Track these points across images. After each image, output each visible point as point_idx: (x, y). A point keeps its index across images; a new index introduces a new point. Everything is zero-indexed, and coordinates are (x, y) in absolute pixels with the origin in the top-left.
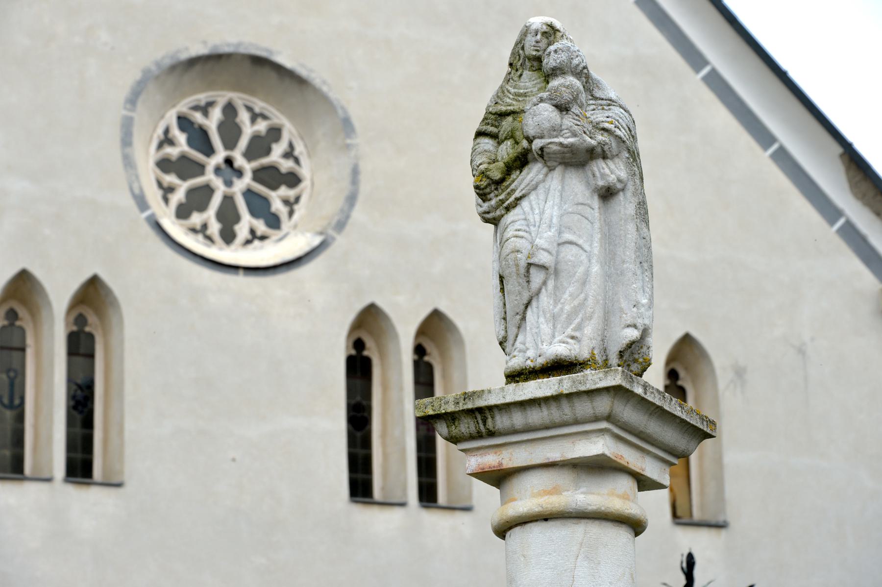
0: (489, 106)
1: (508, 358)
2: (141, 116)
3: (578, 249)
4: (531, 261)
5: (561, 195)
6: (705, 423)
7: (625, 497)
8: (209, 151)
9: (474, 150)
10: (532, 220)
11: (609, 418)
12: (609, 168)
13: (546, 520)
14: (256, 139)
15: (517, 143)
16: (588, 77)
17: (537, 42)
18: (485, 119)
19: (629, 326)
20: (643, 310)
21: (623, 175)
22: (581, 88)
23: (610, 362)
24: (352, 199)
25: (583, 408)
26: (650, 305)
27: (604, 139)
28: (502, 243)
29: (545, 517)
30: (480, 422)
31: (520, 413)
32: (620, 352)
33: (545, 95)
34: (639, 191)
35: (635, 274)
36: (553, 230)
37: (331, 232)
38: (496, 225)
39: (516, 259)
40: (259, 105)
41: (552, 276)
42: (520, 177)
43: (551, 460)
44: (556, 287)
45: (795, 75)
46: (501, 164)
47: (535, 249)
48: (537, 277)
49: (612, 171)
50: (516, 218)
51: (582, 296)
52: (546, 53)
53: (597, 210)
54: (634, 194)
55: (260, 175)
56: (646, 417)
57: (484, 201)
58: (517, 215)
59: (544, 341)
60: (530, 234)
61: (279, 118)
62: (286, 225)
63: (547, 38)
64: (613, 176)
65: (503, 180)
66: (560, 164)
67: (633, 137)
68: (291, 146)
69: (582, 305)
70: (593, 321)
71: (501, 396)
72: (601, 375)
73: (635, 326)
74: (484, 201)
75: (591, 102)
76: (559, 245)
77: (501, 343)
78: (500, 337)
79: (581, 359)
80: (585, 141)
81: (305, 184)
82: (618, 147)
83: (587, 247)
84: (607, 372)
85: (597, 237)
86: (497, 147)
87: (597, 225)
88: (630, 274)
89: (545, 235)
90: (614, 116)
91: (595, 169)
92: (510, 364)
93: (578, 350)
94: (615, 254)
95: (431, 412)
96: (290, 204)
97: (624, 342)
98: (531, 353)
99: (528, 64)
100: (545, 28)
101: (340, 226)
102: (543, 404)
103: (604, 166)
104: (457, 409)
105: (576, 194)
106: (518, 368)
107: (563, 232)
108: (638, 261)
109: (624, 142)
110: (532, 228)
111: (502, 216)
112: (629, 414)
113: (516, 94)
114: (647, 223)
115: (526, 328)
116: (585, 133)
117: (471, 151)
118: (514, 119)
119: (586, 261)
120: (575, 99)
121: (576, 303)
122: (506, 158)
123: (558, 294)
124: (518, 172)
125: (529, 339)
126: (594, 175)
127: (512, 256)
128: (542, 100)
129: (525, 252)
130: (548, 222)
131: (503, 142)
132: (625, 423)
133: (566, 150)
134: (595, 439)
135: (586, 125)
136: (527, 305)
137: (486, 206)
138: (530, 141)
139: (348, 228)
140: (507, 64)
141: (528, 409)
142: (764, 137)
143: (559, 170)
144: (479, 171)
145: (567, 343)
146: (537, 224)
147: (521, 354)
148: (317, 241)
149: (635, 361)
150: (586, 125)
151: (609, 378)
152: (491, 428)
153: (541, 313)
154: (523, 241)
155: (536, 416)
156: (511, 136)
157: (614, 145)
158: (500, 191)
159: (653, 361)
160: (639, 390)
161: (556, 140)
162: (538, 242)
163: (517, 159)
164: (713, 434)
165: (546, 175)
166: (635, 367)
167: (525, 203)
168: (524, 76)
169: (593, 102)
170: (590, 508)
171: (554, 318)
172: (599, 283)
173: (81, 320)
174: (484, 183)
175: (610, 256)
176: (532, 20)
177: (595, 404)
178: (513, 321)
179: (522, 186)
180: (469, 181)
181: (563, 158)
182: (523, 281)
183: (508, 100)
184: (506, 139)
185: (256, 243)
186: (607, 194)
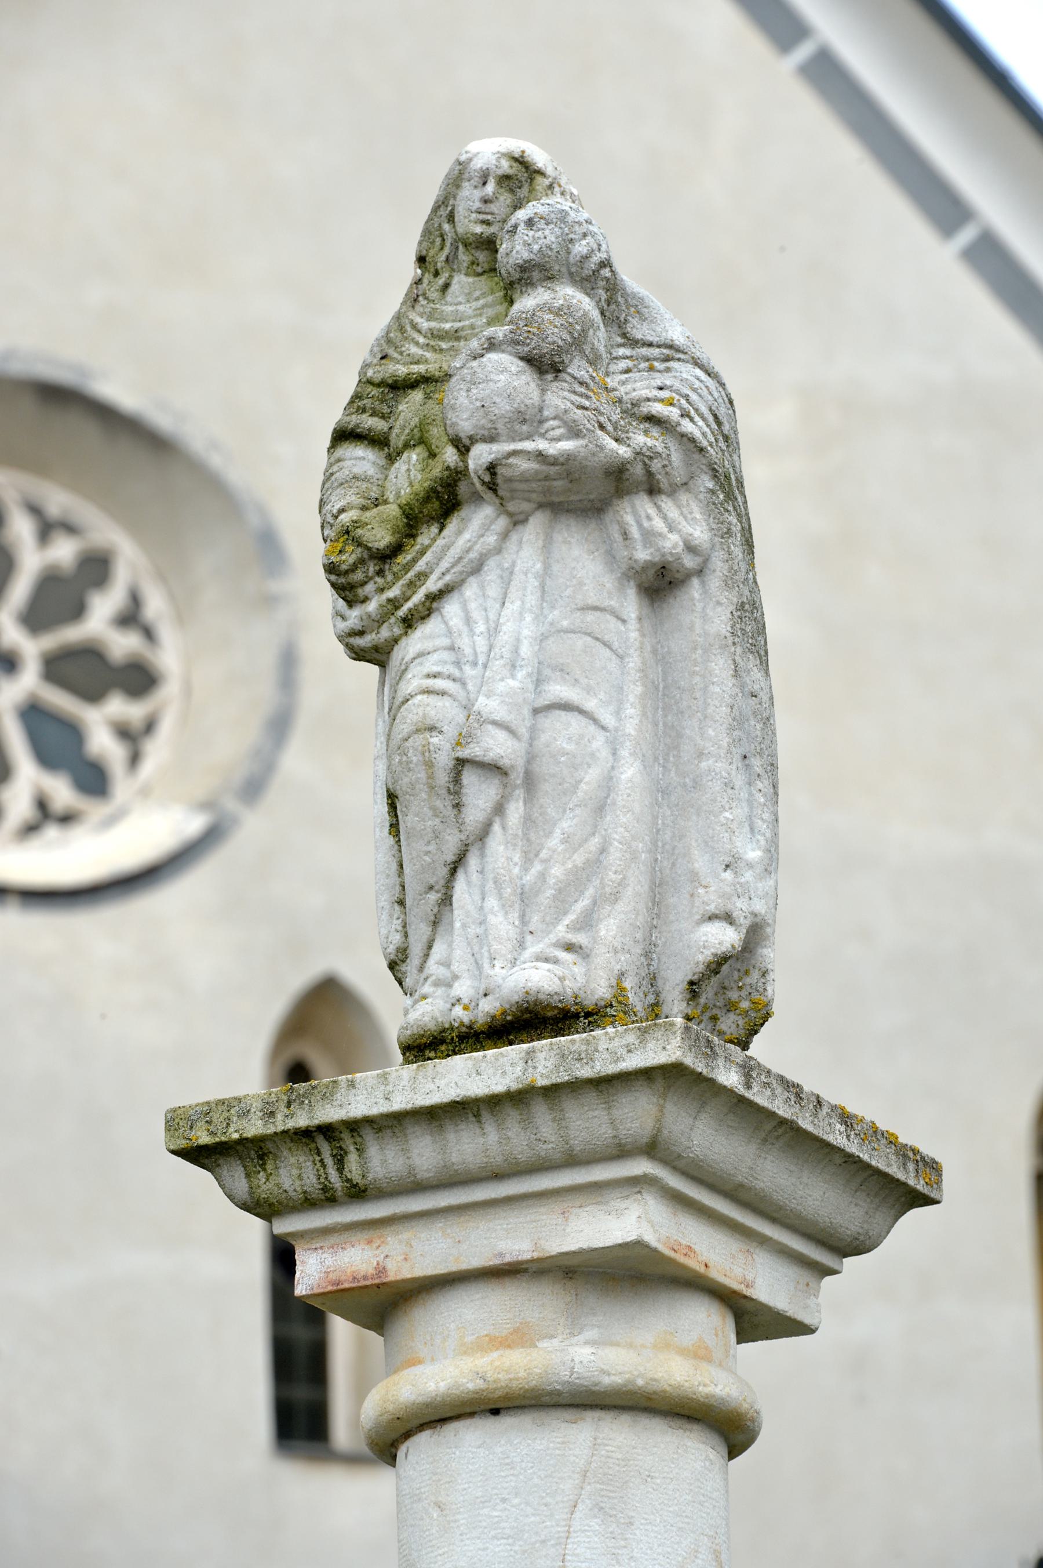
0: (366, 366)
1: (408, 1001)
3: (584, 721)
4: (464, 753)
5: (543, 587)
6: (911, 1166)
7: (699, 1354)
9: (328, 477)
10: (468, 651)
11: (652, 1148)
12: (665, 518)
13: (495, 1412)
15: (432, 455)
16: (613, 287)
17: (486, 201)
18: (357, 397)
19: (712, 918)
20: (748, 876)
21: (700, 533)
22: (595, 314)
23: (665, 1009)
24: (280, 726)
25: (588, 1123)
26: (770, 865)
27: (650, 442)
28: (395, 709)
29: (494, 1406)
30: (329, 1161)
31: (427, 1139)
32: (691, 983)
33: (500, 332)
34: (741, 576)
35: (729, 785)
36: (520, 674)
37: (231, 804)
38: (383, 665)
39: (426, 749)
40: (58, 500)
41: (520, 793)
42: (440, 542)
43: (508, 1259)
44: (528, 821)
46: (392, 510)
47: (475, 721)
48: (480, 796)
49: (672, 525)
50: (429, 645)
51: (595, 842)
52: (508, 226)
53: (633, 625)
54: (728, 583)
56: (752, 1148)
57: (350, 604)
58: (431, 637)
59: (498, 958)
60: (464, 684)
61: (106, 532)
62: (122, 787)
63: (512, 191)
64: (674, 538)
65: (396, 549)
66: (541, 506)
67: (726, 438)
68: (135, 600)
69: (596, 863)
70: (620, 906)
71: (379, 1094)
72: (631, 1038)
73: (728, 918)
74: (350, 604)
75: (622, 351)
76: (536, 711)
77: (392, 966)
78: (392, 949)
79: (589, 1003)
80: (601, 448)
81: (169, 691)
82: (689, 464)
83: (607, 717)
84: (644, 1031)
85: (635, 691)
86: (386, 469)
87: (634, 662)
88: (717, 786)
89: (501, 687)
90: (677, 385)
91: (629, 519)
92: (413, 1016)
93: (581, 980)
94: (680, 736)
95: (205, 1139)
96: (133, 737)
97: (701, 958)
98: (463, 989)
99: (464, 257)
100: (506, 166)
102: (485, 1115)
103: (652, 511)
104: (271, 1130)
105: (581, 584)
106: (432, 1026)
107: (548, 680)
108: (738, 752)
109: (701, 450)
110: (468, 670)
111: (396, 641)
112: (705, 1137)
113: (433, 334)
114: (763, 658)
115: (451, 924)
116: (602, 427)
117: (321, 478)
118: (428, 397)
119: (604, 753)
120: (578, 342)
121: (579, 859)
122: (406, 492)
123: (532, 836)
124: (434, 529)
125: (460, 953)
126: (626, 535)
127: (418, 740)
128: (492, 345)
129: (451, 732)
130: (507, 655)
131: (399, 454)
132: (696, 1163)
133: (553, 470)
134: (618, 1204)
135: (606, 408)
136: (455, 867)
137: (354, 616)
138: (463, 448)
139: (274, 794)
140: (413, 258)
141: (449, 1127)
143: (537, 522)
144: (337, 527)
145: (556, 961)
146: (481, 660)
147: (440, 991)
148: (194, 825)
149: (731, 1007)
150: (606, 408)
151: (651, 1045)
152: (357, 1178)
153: (490, 885)
154: (446, 702)
155: (469, 1145)
156: (420, 440)
157: (676, 458)
158: (390, 577)
159: (775, 1008)
160: (730, 1078)
161: (528, 445)
162: (487, 705)
163: (431, 494)
164: (933, 1195)
165: (505, 536)
166: (730, 1023)
167: (451, 608)
168: (455, 287)
169: (627, 351)
170: (606, 1380)
171: (525, 898)
172: (637, 807)
174: (349, 558)
176: (473, 147)
177: (616, 1113)
179: (445, 564)
181: (548, 491)
182: (444, 804)
183: (414, 350)
184: (407, 446)
185: (52, 832)
186: (660, 583)
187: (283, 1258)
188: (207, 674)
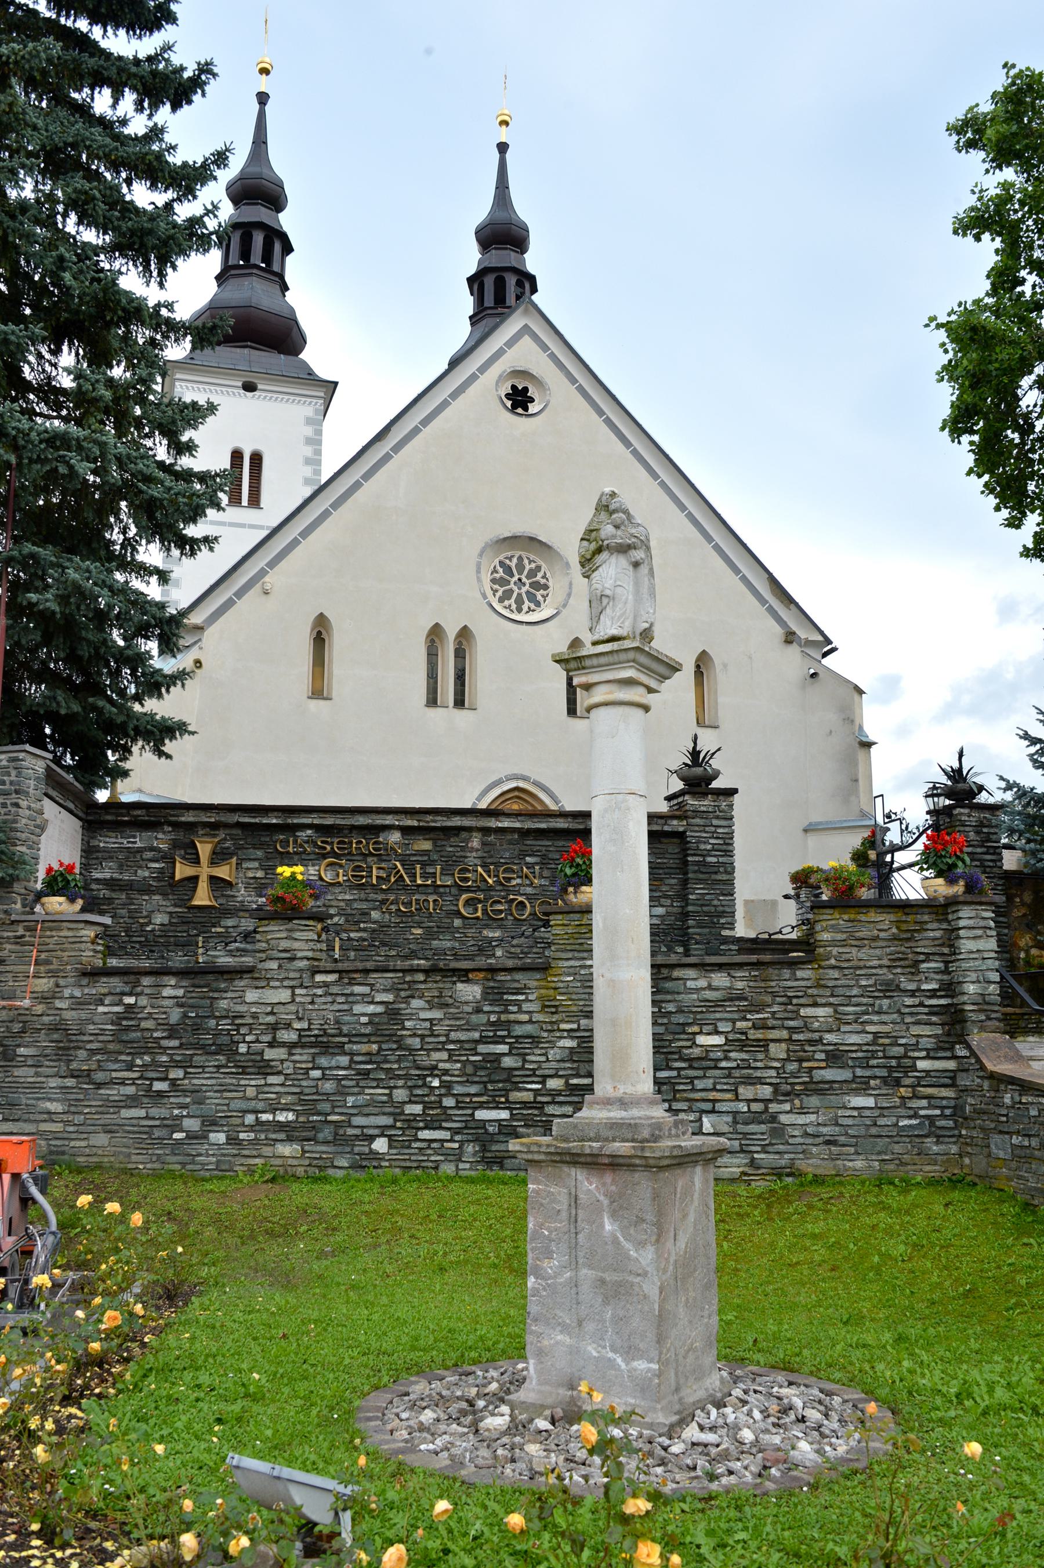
2: (484, 561)
8: (512, 576)
11: (634, 661)
14: (531, 570)
24: (569, 595)
25: (623, 656)
45: (618, 396)
47: (604, 588)
48: (605, 601)
49: (638, 555)
55: (531, 585)
62: (543, 605)
101: (564, 606)
112: (643, 659)
142: (736, 570)
155: (603, 660)
173: (460, 643)
175: (637, 592)
178: (595, 619)
180: (577, 559)
186: (636, 565)
187: (570, 680)
188: (557, 586)
